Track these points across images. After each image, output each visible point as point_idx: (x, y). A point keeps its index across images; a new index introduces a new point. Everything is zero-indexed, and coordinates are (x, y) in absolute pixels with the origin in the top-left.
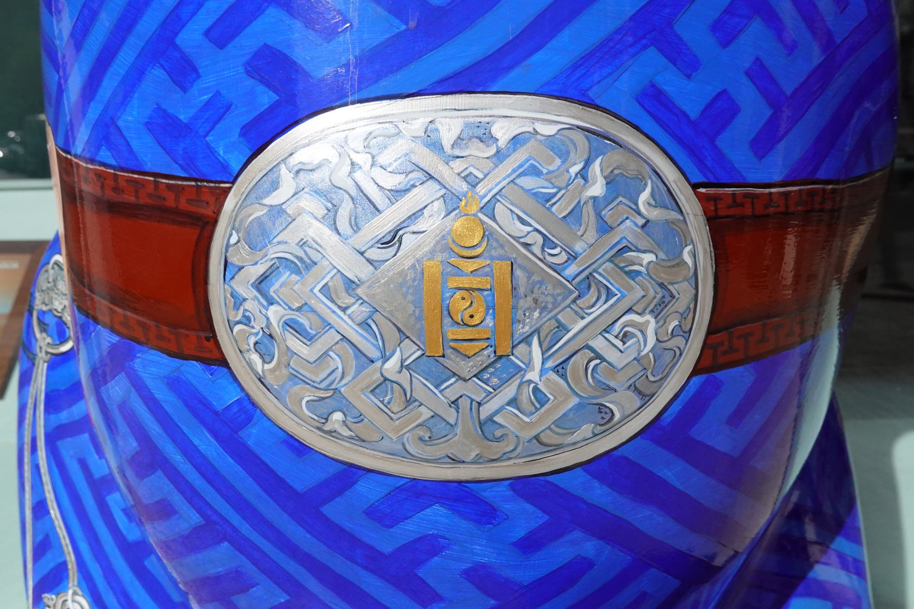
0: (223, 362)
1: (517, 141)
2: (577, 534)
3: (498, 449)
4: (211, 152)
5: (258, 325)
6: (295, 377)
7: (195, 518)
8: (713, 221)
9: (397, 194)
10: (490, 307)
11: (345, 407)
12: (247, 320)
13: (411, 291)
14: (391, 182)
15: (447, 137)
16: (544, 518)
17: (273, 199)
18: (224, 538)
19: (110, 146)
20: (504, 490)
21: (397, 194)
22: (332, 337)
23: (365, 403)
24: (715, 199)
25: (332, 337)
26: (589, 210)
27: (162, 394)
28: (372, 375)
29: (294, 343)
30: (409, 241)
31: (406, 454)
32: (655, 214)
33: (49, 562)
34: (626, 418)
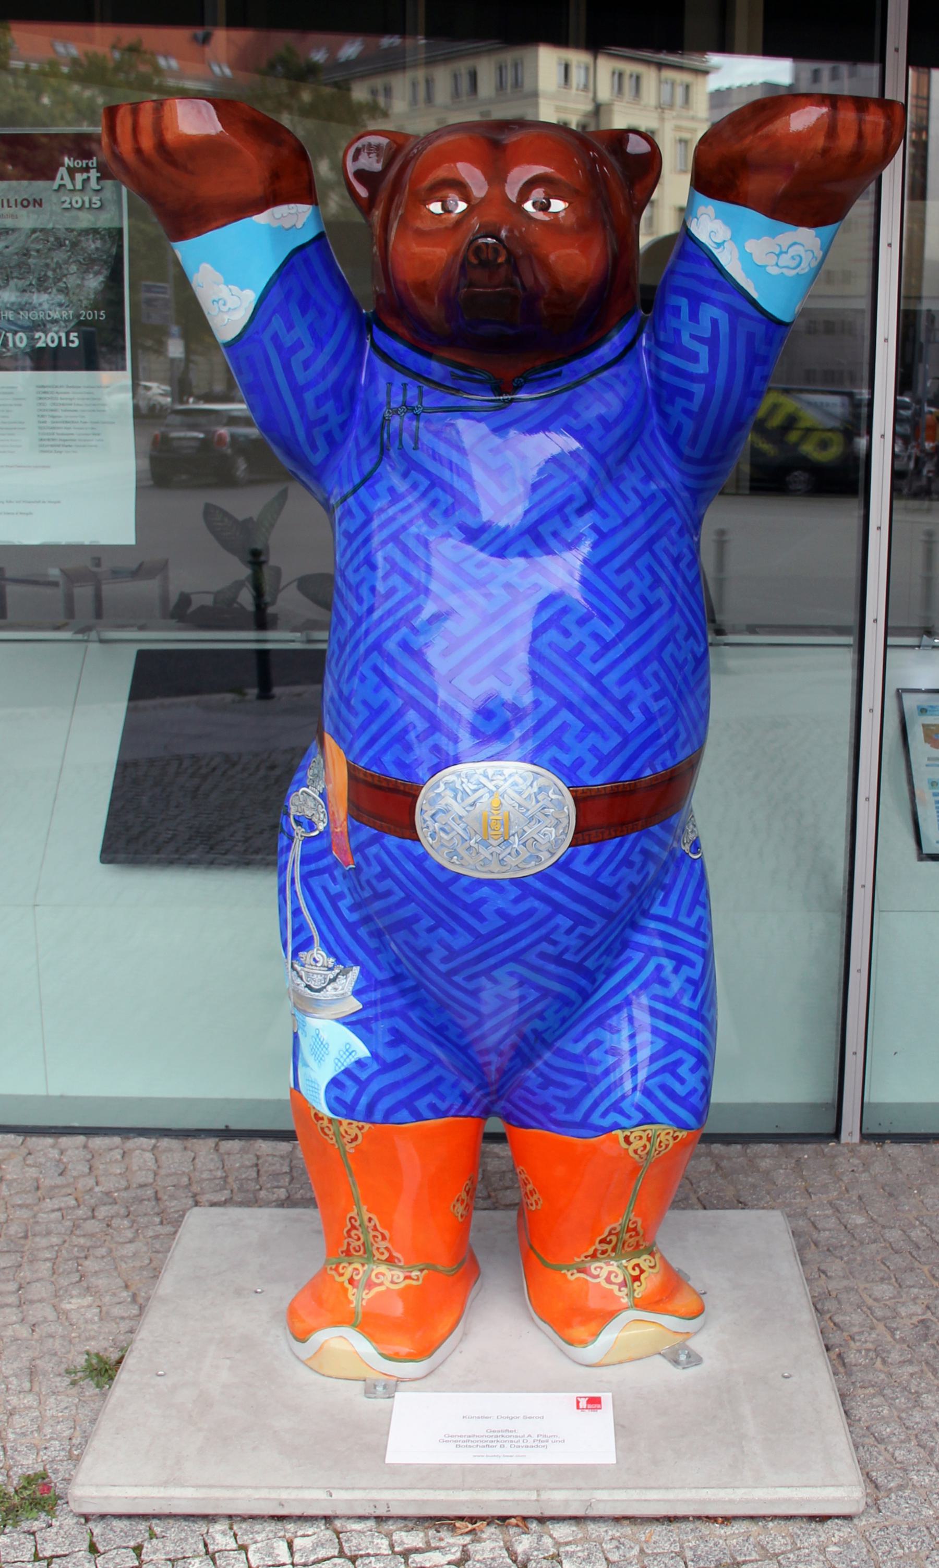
0: (419, 840)
1: (510, 775)
2: (532, 899)
3: (505, 869)
4: (417, 775)
5: (431, 829)
6: (442, 845)
7: (402, 895)
8: (577, 800)
9: (475, 791)
10: (503, 824)
11: (457, 854)
12: (428, 827)
13: (900, 1493)
14: (473, 787)
15: (490, 774)
16: (520, 892)
17: (438, 791)
18: (413, 901)
19: (378, 767)
20: (508, 883)
21: (475, 791)
22: (454, 833)
23: (464, 854)
24: (576, 791)
25: (454, 833)
26: (533, 796)
27: (395, 851)
28: (466, 845)
29: (442, 834)
30: (478, 805)
31: (477, 870)
32: (554, 797)
33: (302, 937)
34: (546, 860)
